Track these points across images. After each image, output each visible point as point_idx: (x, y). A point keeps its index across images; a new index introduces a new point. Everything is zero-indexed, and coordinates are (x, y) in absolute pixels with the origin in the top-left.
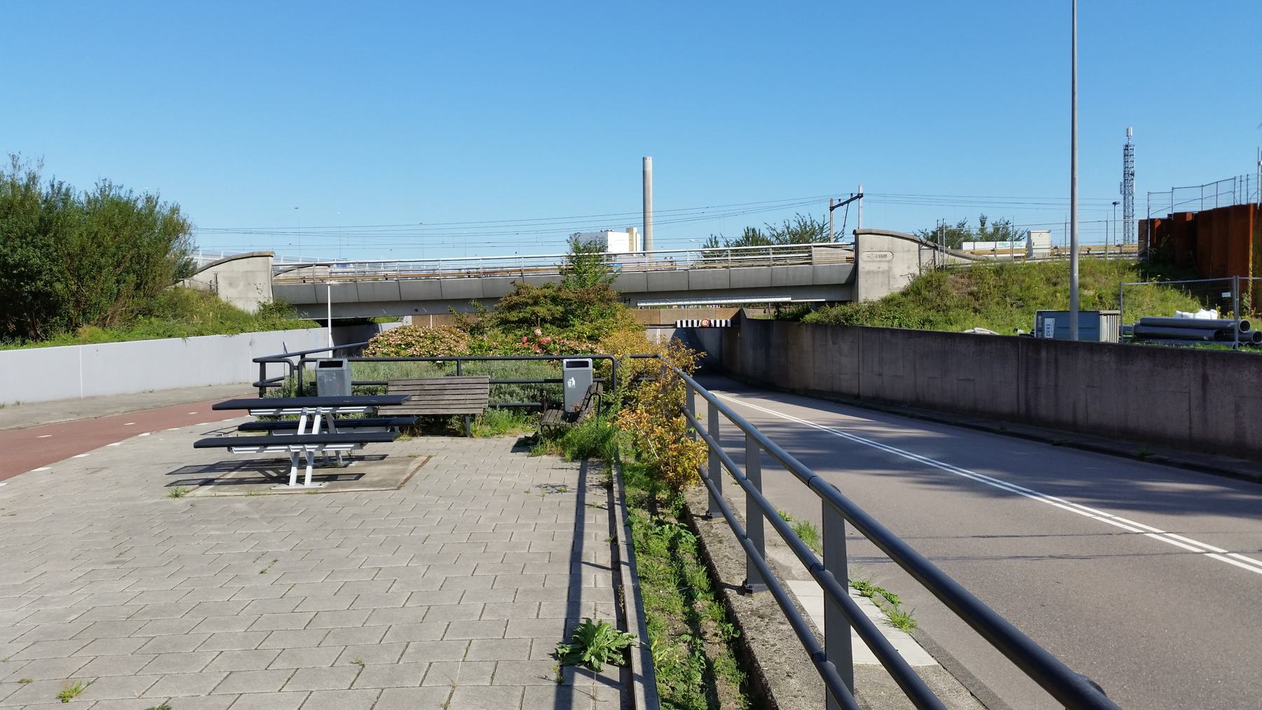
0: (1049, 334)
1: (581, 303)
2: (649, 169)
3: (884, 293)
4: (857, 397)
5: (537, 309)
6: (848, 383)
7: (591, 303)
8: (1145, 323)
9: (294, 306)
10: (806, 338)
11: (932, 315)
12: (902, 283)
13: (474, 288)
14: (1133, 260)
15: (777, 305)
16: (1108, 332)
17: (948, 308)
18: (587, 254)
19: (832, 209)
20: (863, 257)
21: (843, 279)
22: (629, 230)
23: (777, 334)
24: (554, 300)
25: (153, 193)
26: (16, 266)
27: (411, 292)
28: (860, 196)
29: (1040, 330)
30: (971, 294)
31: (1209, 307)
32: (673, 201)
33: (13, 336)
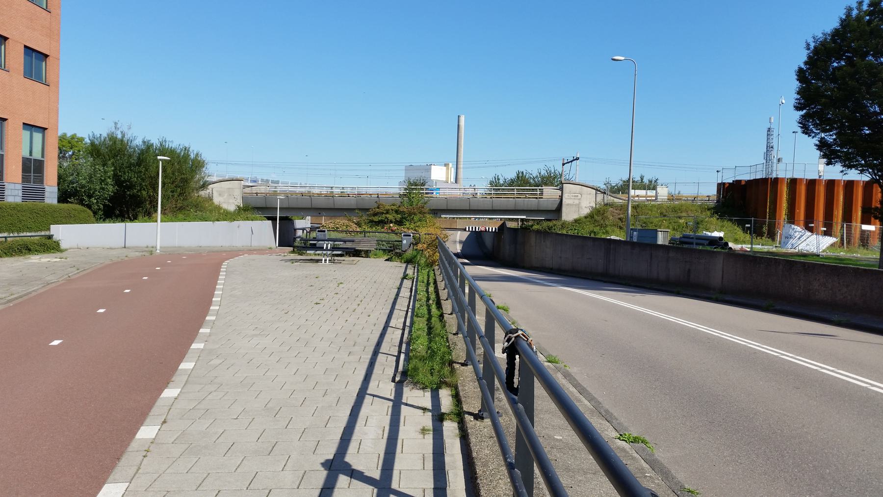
0: (635, 240)
1: (410, 214)
2: (462, 123)
3: (576, 216)
4: (552, 269)
5: (388, 216)
6: (548, 263)
7: (415, 214)
8: (685, 237)
9: (256, 208)
10: (533, 239)
11: (596, 229)
12: (585, 211)
13: (351, 203)
14: (712, 204)
15: (522, 220)
16: (661, 239)
17: (606, 226)
18: (416, 186)
19: (563, 164)
20: (565, 196)
21: (554, 207)
22: (446, 165)
23: (526, 238)
24: (397, 212)
25: (187, 146)
26: (125, 181)
27: (341, 203)
28: (577, 159)
29: (631, 237)
30: (620, 219)
31: (720, 231)
32: (465, 159)
33: (117, 217)
